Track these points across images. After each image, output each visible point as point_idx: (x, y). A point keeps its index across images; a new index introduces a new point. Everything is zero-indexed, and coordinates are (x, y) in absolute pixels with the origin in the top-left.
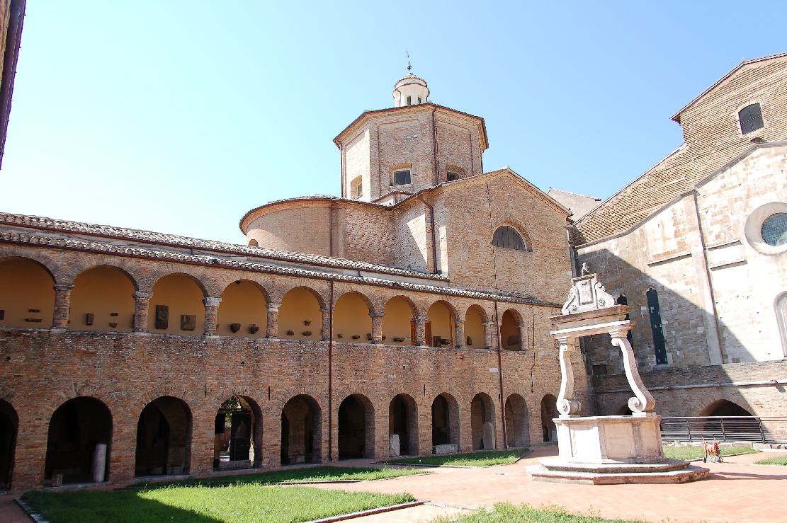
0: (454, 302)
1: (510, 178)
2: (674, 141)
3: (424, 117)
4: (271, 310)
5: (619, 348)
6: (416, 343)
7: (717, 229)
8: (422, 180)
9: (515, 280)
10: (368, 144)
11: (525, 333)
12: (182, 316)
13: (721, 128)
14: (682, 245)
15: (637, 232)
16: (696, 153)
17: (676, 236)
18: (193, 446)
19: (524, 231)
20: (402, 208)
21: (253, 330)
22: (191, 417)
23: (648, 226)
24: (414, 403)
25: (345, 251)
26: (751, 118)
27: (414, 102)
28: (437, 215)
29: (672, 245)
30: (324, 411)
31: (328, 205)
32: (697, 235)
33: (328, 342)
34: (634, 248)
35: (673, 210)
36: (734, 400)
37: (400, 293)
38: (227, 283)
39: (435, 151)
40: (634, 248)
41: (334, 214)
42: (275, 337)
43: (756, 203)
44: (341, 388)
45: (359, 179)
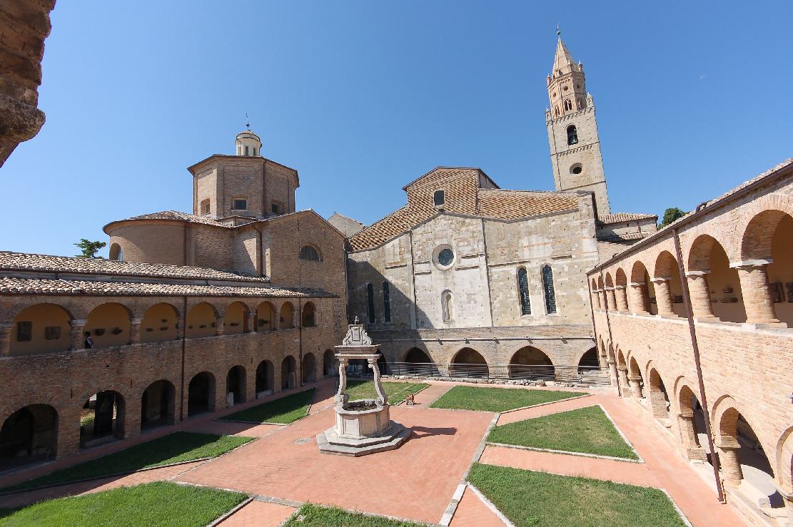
0: (273, 301)
1: (311, 217)
2: (402, 201)
3: (257, 166)
4: (133, 323)
5: (372, 369)
6: (246, 331)
7: (419, 253)
8: (255, 210)
9: (313, 279)
10: (215, 178)
11: (317, 315)
12: (47, 329)
13: (425, 199)
14: (403, 260)
15: (381, 248)
16: (414, 210)
17: (400, 254)
18: (59, 438)
19: (319, 249)
20: (238, 232)
21: (117, 331)
22: (57, 415)
23: (388, 246)
24: (244, 369)
25: (196, 260)
26: (439, 198)
27: (251, 154)
28: (264, 238)
29: (398, 259)
30: (178, 389)
31: (183, 225)
32: (410, 256)
33: (182, 340)
34: (379, 257)
35: (399, 240)
36: (420, 347)
37: (237, 300)
38: (93, 307)
39: (265, 190)
40: (379, 257)
41: (187, 231)
42: (137, 342)
43: (438, 243)
44: (191, 370)
45: (208, 200)
